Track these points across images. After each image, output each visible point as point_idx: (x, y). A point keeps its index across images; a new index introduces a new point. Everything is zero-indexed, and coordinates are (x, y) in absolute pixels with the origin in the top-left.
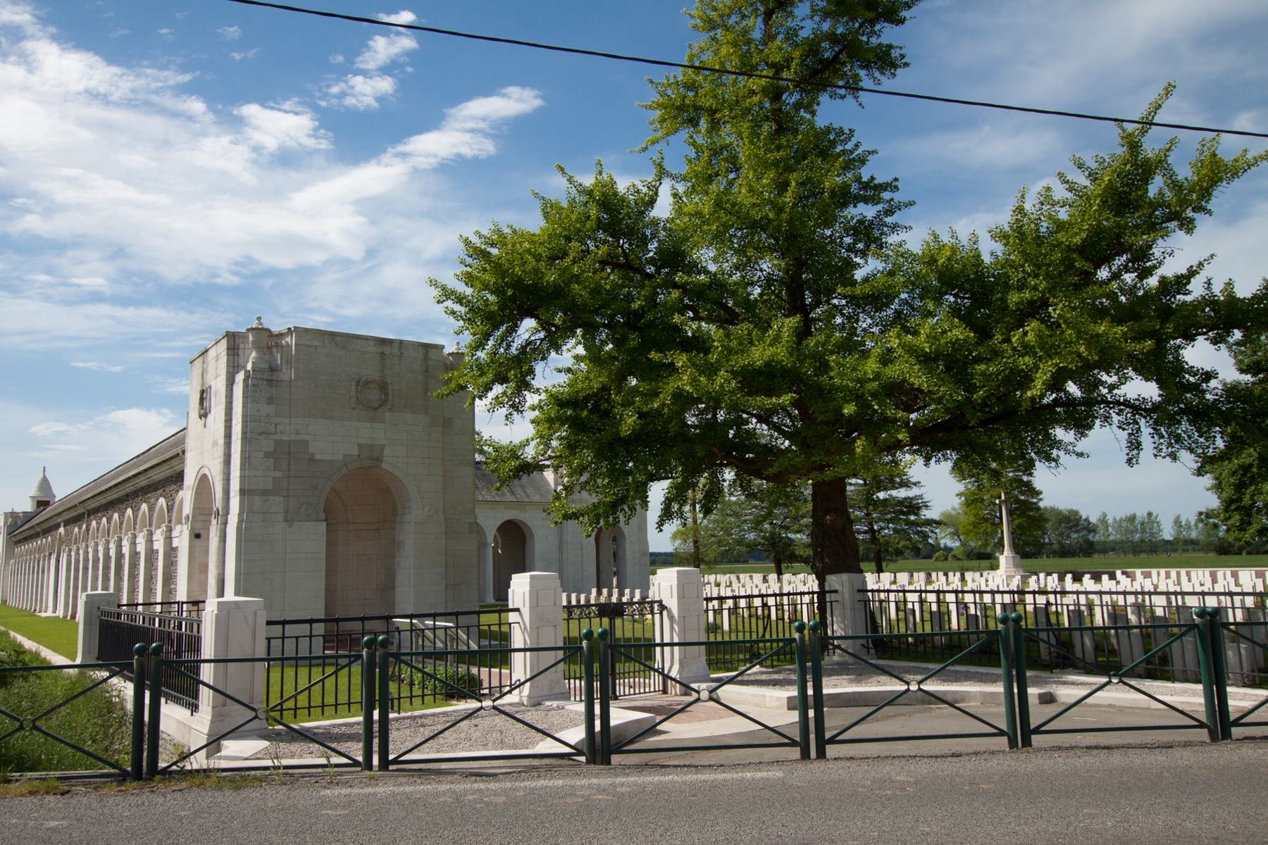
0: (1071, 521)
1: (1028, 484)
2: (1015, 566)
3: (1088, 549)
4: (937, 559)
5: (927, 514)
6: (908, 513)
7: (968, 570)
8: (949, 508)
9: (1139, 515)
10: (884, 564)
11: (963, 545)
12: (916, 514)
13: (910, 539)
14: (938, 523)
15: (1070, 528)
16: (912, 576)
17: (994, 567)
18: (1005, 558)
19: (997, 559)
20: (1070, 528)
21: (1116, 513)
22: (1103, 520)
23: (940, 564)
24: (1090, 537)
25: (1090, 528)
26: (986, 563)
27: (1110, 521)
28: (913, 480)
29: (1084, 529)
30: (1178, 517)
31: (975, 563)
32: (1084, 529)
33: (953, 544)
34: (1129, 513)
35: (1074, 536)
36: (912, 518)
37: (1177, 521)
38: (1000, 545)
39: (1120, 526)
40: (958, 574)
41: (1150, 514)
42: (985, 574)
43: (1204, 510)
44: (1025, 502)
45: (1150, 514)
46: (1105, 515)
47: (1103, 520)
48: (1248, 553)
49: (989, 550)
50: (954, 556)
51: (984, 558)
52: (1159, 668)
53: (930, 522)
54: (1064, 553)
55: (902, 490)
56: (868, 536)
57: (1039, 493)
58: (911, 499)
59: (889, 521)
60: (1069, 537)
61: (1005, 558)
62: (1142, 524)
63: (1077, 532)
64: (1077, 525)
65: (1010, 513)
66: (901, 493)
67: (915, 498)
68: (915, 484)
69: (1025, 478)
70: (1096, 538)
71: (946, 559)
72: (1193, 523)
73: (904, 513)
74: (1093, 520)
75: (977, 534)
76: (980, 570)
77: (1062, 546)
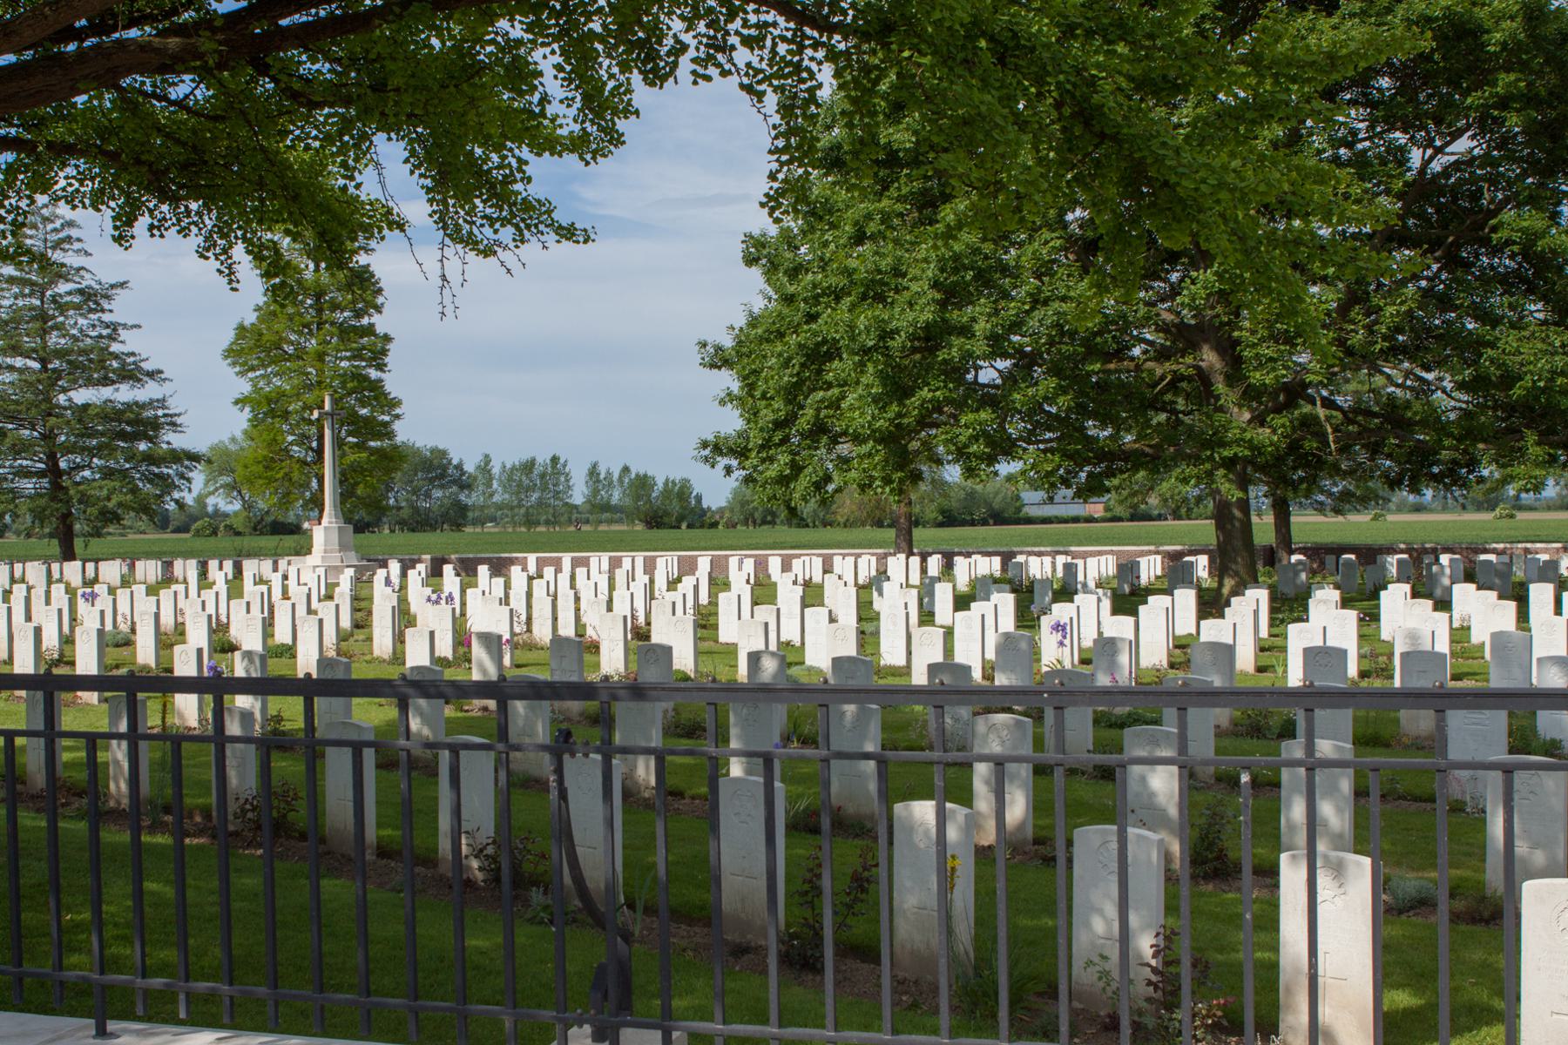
0: (436, 467)
1: (376, 386)
2: (343, 547)
3: (457, 517)
4: (198, 533)
5: (173, 440)
6: (133, 437)
7: (249, 556)
8: (225, 438)
9: (539, 460)
10: (78, 543)
11: (248, 506)
12: (150, 439)
13: (135, 491)
14: (194, 457)
15: (431, 480)
16: (132, 567)
17: (304, 550)
18: (324, 532)
19: (308, 535)
20: (431, 480)
21: (506, 456)
22: (485, 467)
23: (199, 543)
24: (462, 497)
25: (465, 484)
26: (289, 541)
27: (496, 471)
28: (146, 366)
29: (454, 482)
30: (595, 466)
31: (269, 541)
32: (454, 482)
33: (222, 503)
34: (525, 457)
35: (437, 493)
36: (143, 446)
37: (593, 472)
38: (317, 503)
39: (510, 479)
40: (228, 565)
41: (555, 460)
42: (282, 563)
43: (711, 438)
44: (368, 421)
45: (555, 460)
46: (487, 459)
47: (485, 467)
48: (689, 527)
49: (291, 517)
50: (229, 528)
51: (281, 533)
52: (355, 610)
53: (177, 456)
54: (420, 522)
55: (124, 387)
56: (45, 482)
57: (395, 403)
58: (142, 406)
59: (92, 452)
60: (428, 496)
61: (324, 532)
62: (543, 476)
63: (442, 487)
64: (442, 476)
65: (339, 443)
66: (124, 394)
67: (150, 404)
68: (152, 375)
69: (373, 374)
70: (471, 499)
71: (215, 533)
72: (616, 476)
73: (123, 435)
74: (469, 467)
75: (271, 480)
76: (275, 555)
77: (416, 510)
